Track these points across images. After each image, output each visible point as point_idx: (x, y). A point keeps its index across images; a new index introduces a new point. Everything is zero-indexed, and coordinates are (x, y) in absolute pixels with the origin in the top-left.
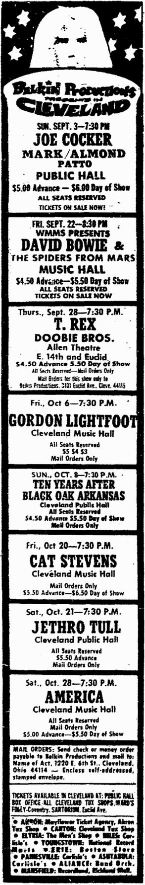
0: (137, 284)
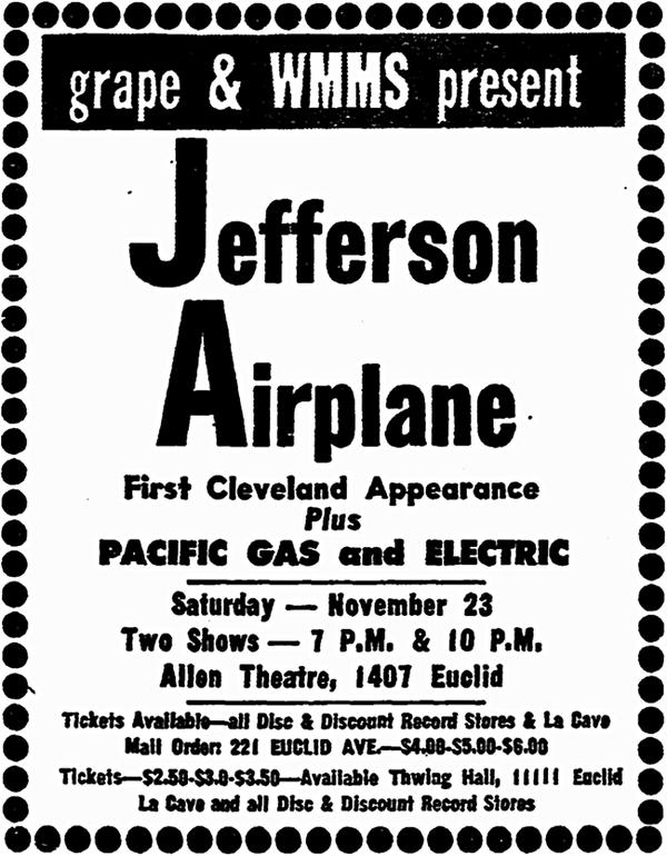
0: (254, 411)
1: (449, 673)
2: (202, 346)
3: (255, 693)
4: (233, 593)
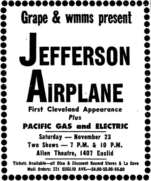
1: (101, 152)
2: (37, 79)
3: (58, 157)
4: (53, 134)
